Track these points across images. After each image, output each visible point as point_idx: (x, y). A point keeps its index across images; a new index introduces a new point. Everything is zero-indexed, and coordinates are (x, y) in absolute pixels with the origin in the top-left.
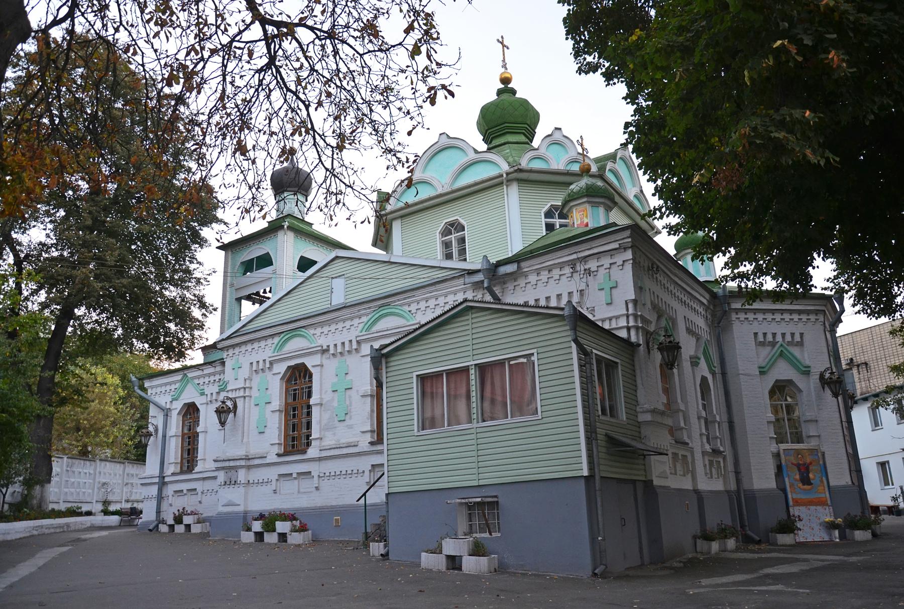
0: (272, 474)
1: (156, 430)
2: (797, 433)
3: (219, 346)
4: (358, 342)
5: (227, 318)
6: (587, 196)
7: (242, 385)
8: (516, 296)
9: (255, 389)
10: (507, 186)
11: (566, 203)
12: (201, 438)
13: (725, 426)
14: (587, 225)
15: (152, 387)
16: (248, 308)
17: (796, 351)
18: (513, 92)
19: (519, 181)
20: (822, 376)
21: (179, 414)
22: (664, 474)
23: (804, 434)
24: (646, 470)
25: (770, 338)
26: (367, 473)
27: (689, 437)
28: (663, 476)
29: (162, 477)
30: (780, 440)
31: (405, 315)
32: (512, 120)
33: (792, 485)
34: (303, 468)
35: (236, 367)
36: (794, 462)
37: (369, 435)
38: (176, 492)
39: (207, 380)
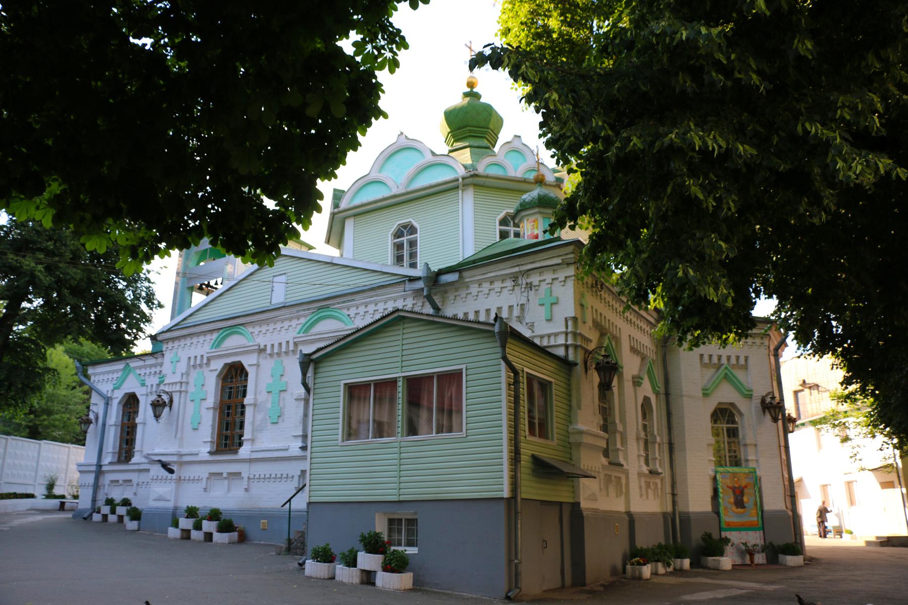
0: (202, 472)
1: (97, 418)
3: (159, 338)
6: (538, 206)
7: (179, 380)
8: (455, 308)
10: (463, 191)
11: (518, 212)
12: (139, 429)
13: (666, 448)
14: (537, 237)
16: (198, 299)
18: (477, 96)
19: (475, 185)
20: (763, 401)
21: (119, 403)
22: (594, 497)
24: (575, 491)
25: (715, 360)
26: (296, 478)
27: (626, 459)
29: (99, 466)
30: (719, 464)
31: (344, 319)
33: (726, 508)
36: (730, 485)
38: (112, 481)
39: (148, 371)
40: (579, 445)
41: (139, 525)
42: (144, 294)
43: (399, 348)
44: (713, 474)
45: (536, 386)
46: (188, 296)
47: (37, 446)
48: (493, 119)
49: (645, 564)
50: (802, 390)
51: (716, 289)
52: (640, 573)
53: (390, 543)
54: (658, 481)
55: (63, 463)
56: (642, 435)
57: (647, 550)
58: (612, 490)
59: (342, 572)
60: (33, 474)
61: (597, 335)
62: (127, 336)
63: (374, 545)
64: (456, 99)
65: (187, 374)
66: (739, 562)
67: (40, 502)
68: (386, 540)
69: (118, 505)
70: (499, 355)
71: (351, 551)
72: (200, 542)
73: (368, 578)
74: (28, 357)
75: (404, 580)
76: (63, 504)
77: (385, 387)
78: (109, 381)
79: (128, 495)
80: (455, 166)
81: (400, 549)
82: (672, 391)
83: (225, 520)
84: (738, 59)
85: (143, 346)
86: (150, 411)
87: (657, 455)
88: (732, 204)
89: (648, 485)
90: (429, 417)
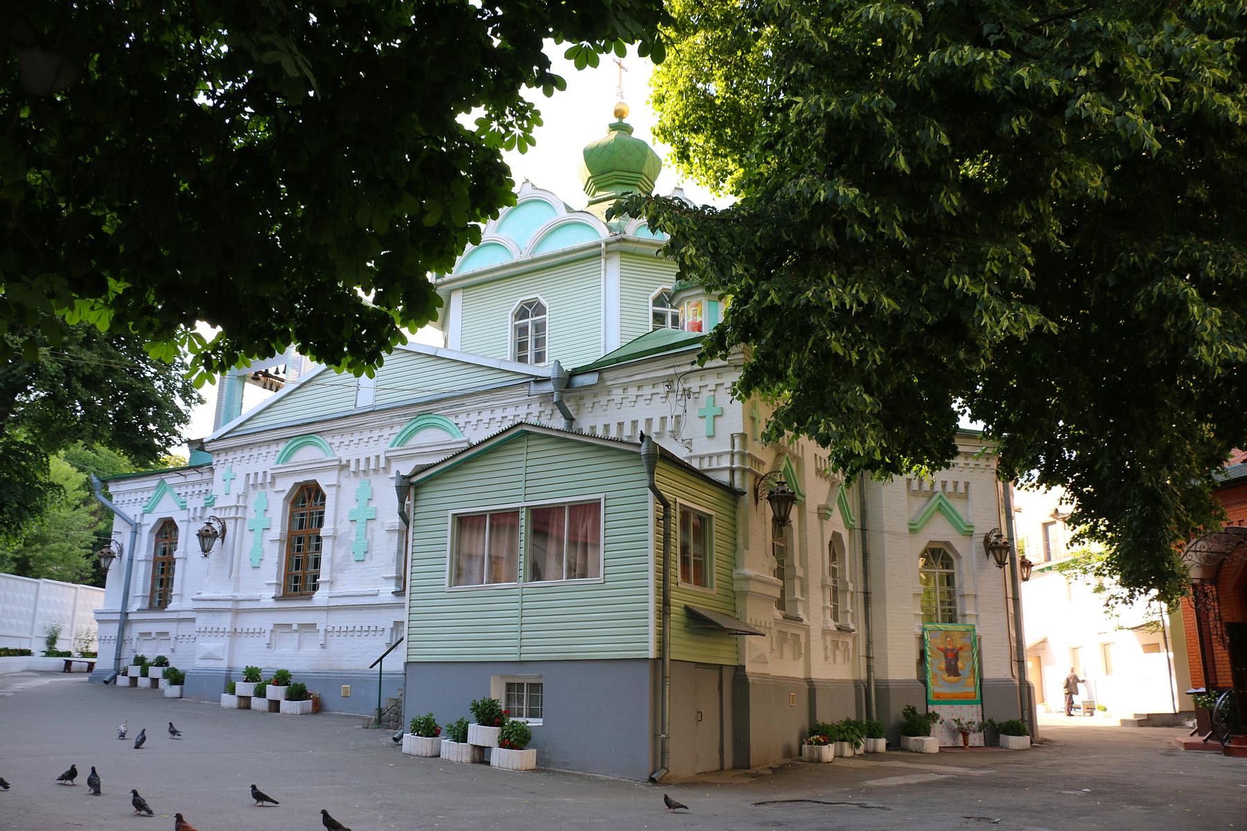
1: (121, 551)
2: (950, 611)
3: (207, 449)
4: (387, 458)
5: (224, 404)
9: (251, 509)
12: (178, 566)
13: (861, 597)
15: (118, 493)
17: (957, 505)
19: (622, 252)
20: (987, 540)
22: (763, 658)
23: (958, 613)
24: (739, 651)
26: (388, 632)
27: (806, 611)
28: (762, 660)
29: (125, 614)
30: (928, 617)
31: (451, 428)
32: (624, 166)
33: (935, 676)
34: (307, 618)
35: (228, 477)
36: (941, 646)
37: (393, 582)
38: (142, 634)
39: (190, 490)
40: (745, 594)
41: (182, 690)
42: (179, 385)
43: (522, 471)
44: (920, 632)
45: (692, 520)
46: (238, 387)
47: (34, 586)
48: (649, 162)
49: (825, 744)
50: (1054, 523)
51: (863, 442)
52: (820, 755)
53: (509, 713)
54: (850, 641)
55: (76, 612)
56: (829, 581)
57: (832, 726)
58: (787, 650)
59: (450, 749)
60: (29, 623)
61: (773, 454)
62: (156, 441)
63: (489, 715)
64: (601, 135)
65: (245, 495)
66: (949, 743)
67: (39, 660)
68: (503, 709)
69: (151, 665)
70: (646, 483)
71: (460, 723)
72: (263, 712)
73: (481, 756)
74: (24, 468)
75: (523, 759)
76: (68, 663)
77: (503, 520)
78: (136, 503)
79: (164, 652)
80: (596, 227)
81: (520, 720)
82: (871, 525)
83: (296, 685)
84: (883, 211)
85: (180, 453)
86: (195, 543)
87: (849, 608)
88: (877, 357)
89: (836, 645)
90: (559, 553)
